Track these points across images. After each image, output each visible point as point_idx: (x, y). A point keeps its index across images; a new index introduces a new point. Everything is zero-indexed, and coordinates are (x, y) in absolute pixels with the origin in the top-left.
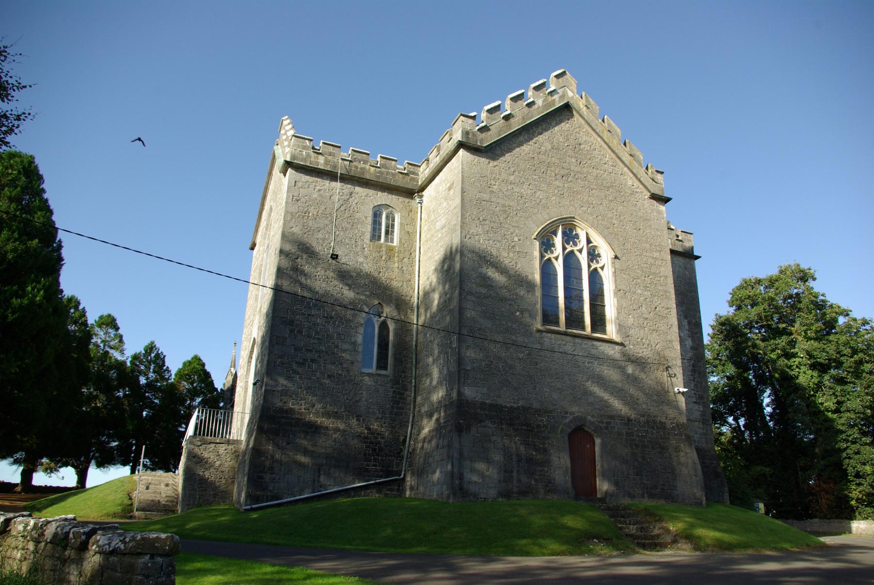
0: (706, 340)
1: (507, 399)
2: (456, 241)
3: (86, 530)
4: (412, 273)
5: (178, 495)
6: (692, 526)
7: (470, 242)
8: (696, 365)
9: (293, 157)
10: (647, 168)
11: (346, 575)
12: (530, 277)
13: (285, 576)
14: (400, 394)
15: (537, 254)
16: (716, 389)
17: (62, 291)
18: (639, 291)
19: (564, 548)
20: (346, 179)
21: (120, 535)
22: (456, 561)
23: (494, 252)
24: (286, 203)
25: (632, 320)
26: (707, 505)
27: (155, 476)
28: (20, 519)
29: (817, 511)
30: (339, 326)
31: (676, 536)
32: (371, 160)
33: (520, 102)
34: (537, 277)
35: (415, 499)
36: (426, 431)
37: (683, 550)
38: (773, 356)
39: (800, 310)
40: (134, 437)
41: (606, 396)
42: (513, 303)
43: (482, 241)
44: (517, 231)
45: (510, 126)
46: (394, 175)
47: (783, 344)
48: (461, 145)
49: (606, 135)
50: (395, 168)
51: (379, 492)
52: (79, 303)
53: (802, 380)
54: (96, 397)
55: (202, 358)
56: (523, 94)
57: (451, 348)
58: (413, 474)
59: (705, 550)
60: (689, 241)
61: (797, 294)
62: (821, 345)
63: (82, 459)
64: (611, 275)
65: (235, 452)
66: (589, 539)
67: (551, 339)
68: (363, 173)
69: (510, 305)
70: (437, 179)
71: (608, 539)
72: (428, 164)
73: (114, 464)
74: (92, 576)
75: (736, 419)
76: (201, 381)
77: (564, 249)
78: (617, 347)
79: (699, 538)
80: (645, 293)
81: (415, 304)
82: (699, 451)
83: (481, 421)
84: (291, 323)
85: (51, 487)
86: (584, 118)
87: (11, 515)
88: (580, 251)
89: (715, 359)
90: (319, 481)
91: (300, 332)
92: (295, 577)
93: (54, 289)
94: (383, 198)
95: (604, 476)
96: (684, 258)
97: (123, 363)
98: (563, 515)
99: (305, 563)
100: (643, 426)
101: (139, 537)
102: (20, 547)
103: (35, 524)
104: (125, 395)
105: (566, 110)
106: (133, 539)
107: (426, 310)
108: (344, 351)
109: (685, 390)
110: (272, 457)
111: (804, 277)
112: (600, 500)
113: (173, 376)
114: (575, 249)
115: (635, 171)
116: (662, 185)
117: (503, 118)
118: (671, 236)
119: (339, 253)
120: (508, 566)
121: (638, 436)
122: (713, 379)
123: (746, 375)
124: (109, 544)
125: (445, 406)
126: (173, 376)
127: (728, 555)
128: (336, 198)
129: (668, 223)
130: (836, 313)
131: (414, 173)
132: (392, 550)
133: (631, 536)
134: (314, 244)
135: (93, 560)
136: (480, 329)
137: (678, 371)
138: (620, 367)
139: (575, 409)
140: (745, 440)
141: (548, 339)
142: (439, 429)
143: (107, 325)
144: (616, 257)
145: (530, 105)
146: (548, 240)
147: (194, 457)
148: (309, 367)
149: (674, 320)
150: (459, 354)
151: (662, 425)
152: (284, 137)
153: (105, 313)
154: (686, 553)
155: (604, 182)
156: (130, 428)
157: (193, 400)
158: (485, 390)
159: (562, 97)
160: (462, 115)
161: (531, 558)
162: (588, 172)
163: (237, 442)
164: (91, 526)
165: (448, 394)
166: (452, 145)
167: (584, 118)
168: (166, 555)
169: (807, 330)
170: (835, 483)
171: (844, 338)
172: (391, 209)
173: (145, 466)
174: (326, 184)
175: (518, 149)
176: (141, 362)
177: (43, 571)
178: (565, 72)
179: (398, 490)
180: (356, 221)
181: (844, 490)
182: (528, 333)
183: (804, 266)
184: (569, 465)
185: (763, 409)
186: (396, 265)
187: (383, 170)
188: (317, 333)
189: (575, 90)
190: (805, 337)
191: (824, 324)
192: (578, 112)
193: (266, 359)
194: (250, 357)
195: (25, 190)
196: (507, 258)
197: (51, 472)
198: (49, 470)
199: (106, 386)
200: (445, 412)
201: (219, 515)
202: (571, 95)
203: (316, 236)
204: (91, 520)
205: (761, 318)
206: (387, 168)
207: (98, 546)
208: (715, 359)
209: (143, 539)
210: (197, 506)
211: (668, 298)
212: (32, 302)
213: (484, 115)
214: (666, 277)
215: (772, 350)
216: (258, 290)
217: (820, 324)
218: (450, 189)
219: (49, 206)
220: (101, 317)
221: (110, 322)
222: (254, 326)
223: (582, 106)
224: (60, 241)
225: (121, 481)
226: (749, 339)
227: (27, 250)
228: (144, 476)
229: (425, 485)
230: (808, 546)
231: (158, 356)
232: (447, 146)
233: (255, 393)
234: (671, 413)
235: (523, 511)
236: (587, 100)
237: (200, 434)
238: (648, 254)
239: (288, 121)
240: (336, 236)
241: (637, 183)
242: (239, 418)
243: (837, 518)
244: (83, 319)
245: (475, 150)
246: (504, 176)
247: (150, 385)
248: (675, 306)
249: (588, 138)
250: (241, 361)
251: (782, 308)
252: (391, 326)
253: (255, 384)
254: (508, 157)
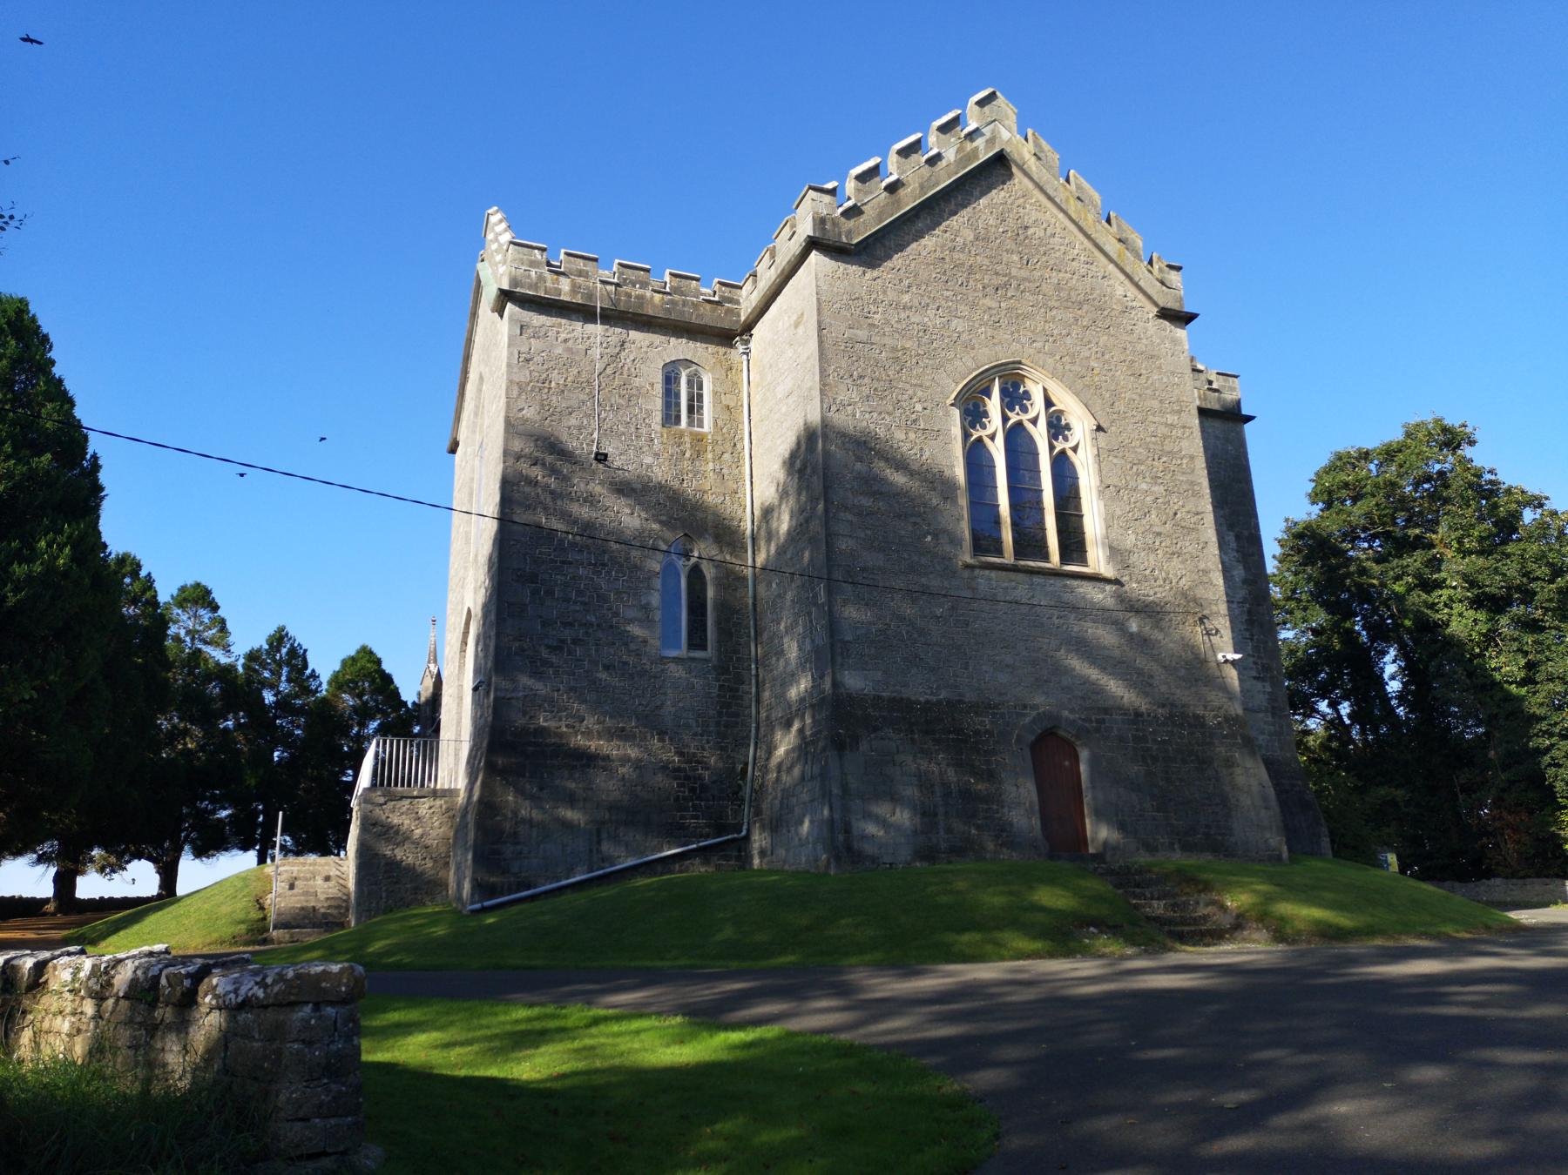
0: (1271, 566)
1: (918, 689)
2: (815, 417)
3: (191, 969)
4: (738, 479)
5: (348, 895)
6: (1269, 899)
7: (840, 419)
8: (1253, 611)
9: (515, 282)
10: (1151, 263)
11: (659, 1014)
12: (947, 473)
13: (552, 1024)
14: (731, 690)
15: (957, 431)
16: (1292, 652)
17: (105, 546)
18: (1144, 486)
19: (1037, 945)
20: (613, 317)
21: (255, 973)
22: (852, 976)
23: (881, 432)
24: (509, 365)
25: (1133, 537)
26: (1292, 860)
27: (304, 864)
28: (66, 959)
29: (1498, 864)
30: (617, 579)
31: (1239, 916)
32: (655, 282)
33: (914, 157)
34: (960, 473)
35: (771, 872)
36: (781, 751)
37: (1254, 941)
38: (1399, 588)
39: (1446, 501)
40: (259, 799)
41: (1093, 674)
42: (919, 520)
43: (856, 415)
44: (920, 393)
45: (898, 204)
46: (695, 305)
47: (1418, 564)
48: (812, 244)
49: (1073, 207)
50: (698, 294)
51: (706, 862)
52: (139, 566)
53: (1457, 628)
54: (185, 733)
55: (375, 650)
56: (918, 142)
57: (815, 604)
58: (763, 828)
59: (1294, 942)
60: (1232, 389)
61: (1441, 473)
62: (1490, 562)
63: (167, 845)
64: (1091, 460)
65: (448, 810)
66: (1081, 927)
67: (990, 579)
68: (641, 306)
69: (915, 524)
70: (773, 308)
71: (1115, 927)
72: (755, 282)
73: (226, 850)
74: (208, 1051)
75: (1333, 705)
76: (376, 691)
77: (1005, 419)
78: (1108, 587)
79: (1283, 919)
80: (1155, 489)
81: (748, 532)
82: (1269, 764)
83: (875, 729)
84: (533, 578)
85: (111, 899)
86: (1031, 178)
87: (46, 954)
88: (1034, 421)
89: (1288, 599)
90: (599, 851)
91: (550, 593)
92: (570, 1023)
93: (91, 543)
94: (678, 348)
95: (1099, 815)
96: (1224, 423)
97: (230, 669)
98: (1031, 888)
99: (589, 999)
100: (1163, 724)
101: (290, 974)
102: (68, 1010)
103: (94, 966)
104: (238, 726)
105: (999, 166)
106: (281, 977)
107: (769, 540)
108: (631, 621)
109: (1238, 656)
110: (515, 813)
111: (1452, 439)
112: (1095, 857)
113: (325, 686)
114: (1024, 418)
115: (1128, 270)
116: (1180, 290)
117: (887, 188)
118: (1198, 384)
119: (609, 450)
120: (941, 981)
121: (1155, 741)
122: (1286, 634)
123: (1348, 625)
124: (236, 991)
125: (812, 706)
126: (325, 686)
127: (1339, 948)
128: (596, 352)
129: (1192, 359)
130: (1518, 502)
131: (731, 301)
132: (734, 965)
133: (1156, 919)
134: (564, 437)
135: (208, 1022)
136: (864, 569)
137: (1223, 623)
138: (1115, 622)
139: (1039, 699)
140: (1353, 741)
141: (985, 580)
142: (804, 749)
143: (195, 602)
144: (1099, 428)
145: (933, 161)
146: (976, 406)
147: (374, 825)
148: (569, 653)
149: (1210, 533)
150: (830, 611)
151: (1199, 722)
152: (494, 246)
153: (190, 582)
154: (1261, 947)
155: (1073, 293)
156: (253, 782)
157: (363, 725)
158: (879, 675)
159: (991, 141)
160: (811, 188)
161: (981, 965)
162: (1042, 278)
163: (450, 793)
164: (200, 961)
165: (816, 686)
166: (796, 245)
167: (1031, 178)
168: (343, 1001)
169: (1463, 536)
170: (1531, 812)
171: (1535, 547)
172: (694, 367)
173: (283, 848)
174: (579, 328)
175: (914, 245)
176: (264, 665)
177: (115, 1050)
178: (994, 93)
179: (738, 858)
180: (634, 392)
181: (1549, 824)
182: (949, 571)
183: (1452, 421)
184: (1035, 798)
185: (1384, 684)
186: (711, 466)
187: (677, 297)
188: (580, 593)
189: (1014, 127)
190: (1459, 551)
191: (1495, 524)
192: (1021, 168)
193: (492, 645)
194: (464, 642)
195: (16, 363)
196: (905, 441)
197: (113, 871)
198: (111, 868)
199: (200, 709)
200: (813, 717)
201: (428, 921)
202: (1008, 136)
203: (565, 423)
204: (191, 952)
205: (1373, 523)
206: (682, 294)
207: (216, 997)
208: (1288, 599)
209: (298, 976)
210: (385, 912)
211: (1196, 494)
212: (50, 568)
213: (850, 186)
214: (1192, 458)
215: (1397, 579)
216: (469, 523)
217: (1488, 525)
218: (797, 325)
219: (65, 392)
220: (183, 589)
221: (198, 597)
222: (467, 585)
223: (1027, 156)
224: (95, 457)
225: (243, 878)
226: (1351, 559)
227: (32, 475)
228: (284, 867)
229: (784, 848)
230: (1488, 928)
231: (293, 652)
232: (788, 247)
233: (477, 703)
234: (1216, 698)
235: (961, 885)
236: (1037, 145)
237: (382, 784)
238: (1156, 419)
239: (499, 216)
240: (601, 421)
241: (1132, 292)
242: (451, 751)
243: (1538, 876)
244: (148, 595)
245: (837, 251)
246: (891, 295)
247: (283, 704)
248: (1210, 508)
249: (1040, 216)
250: (447, 649)
251: (1414, 498)
252: (709, 572)
253: (475, 689)
254: (897, 260)
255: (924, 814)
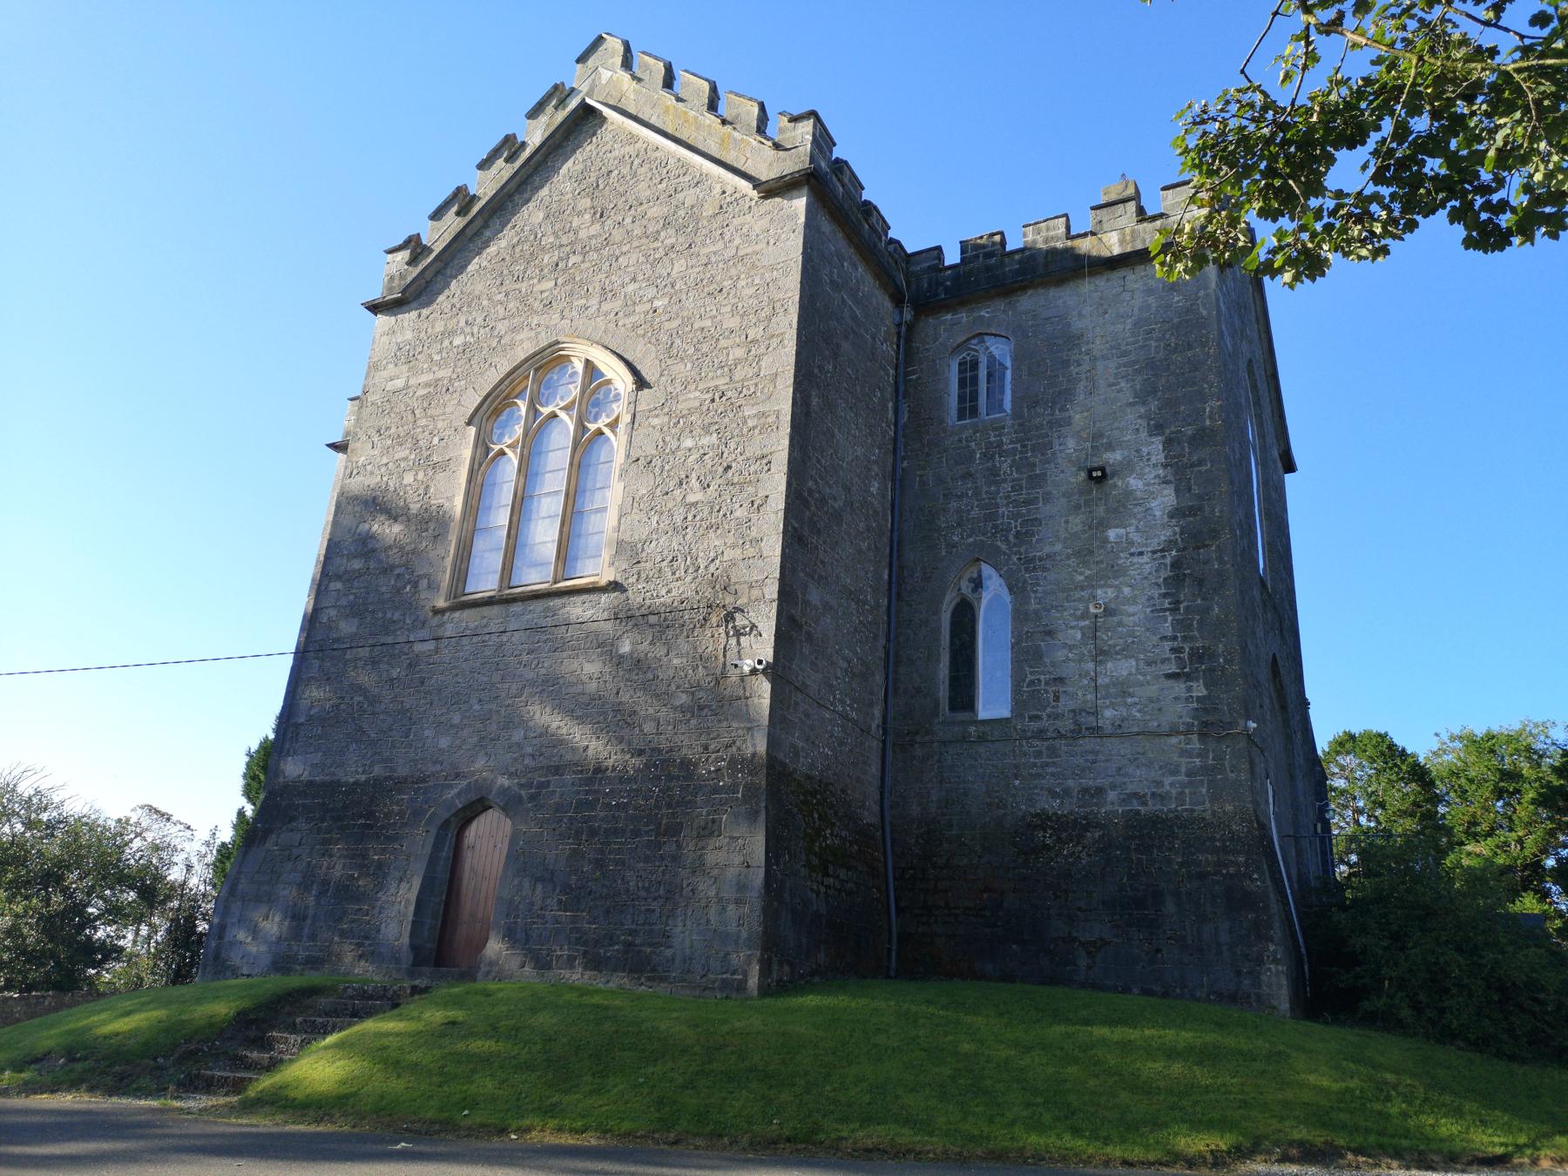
26: (765, 991)
255: (293, 917)
